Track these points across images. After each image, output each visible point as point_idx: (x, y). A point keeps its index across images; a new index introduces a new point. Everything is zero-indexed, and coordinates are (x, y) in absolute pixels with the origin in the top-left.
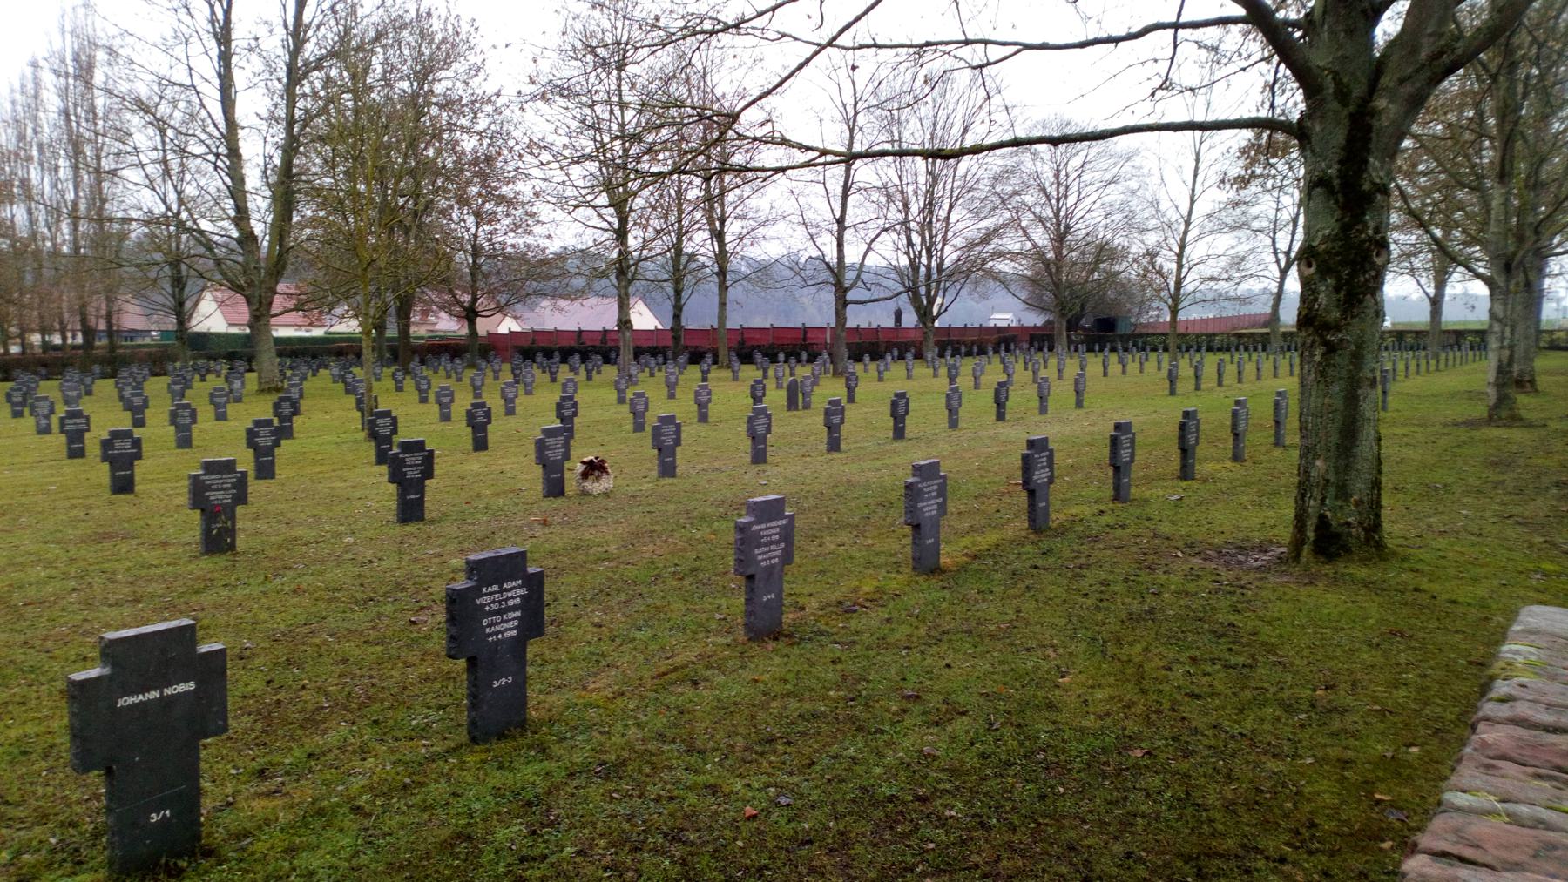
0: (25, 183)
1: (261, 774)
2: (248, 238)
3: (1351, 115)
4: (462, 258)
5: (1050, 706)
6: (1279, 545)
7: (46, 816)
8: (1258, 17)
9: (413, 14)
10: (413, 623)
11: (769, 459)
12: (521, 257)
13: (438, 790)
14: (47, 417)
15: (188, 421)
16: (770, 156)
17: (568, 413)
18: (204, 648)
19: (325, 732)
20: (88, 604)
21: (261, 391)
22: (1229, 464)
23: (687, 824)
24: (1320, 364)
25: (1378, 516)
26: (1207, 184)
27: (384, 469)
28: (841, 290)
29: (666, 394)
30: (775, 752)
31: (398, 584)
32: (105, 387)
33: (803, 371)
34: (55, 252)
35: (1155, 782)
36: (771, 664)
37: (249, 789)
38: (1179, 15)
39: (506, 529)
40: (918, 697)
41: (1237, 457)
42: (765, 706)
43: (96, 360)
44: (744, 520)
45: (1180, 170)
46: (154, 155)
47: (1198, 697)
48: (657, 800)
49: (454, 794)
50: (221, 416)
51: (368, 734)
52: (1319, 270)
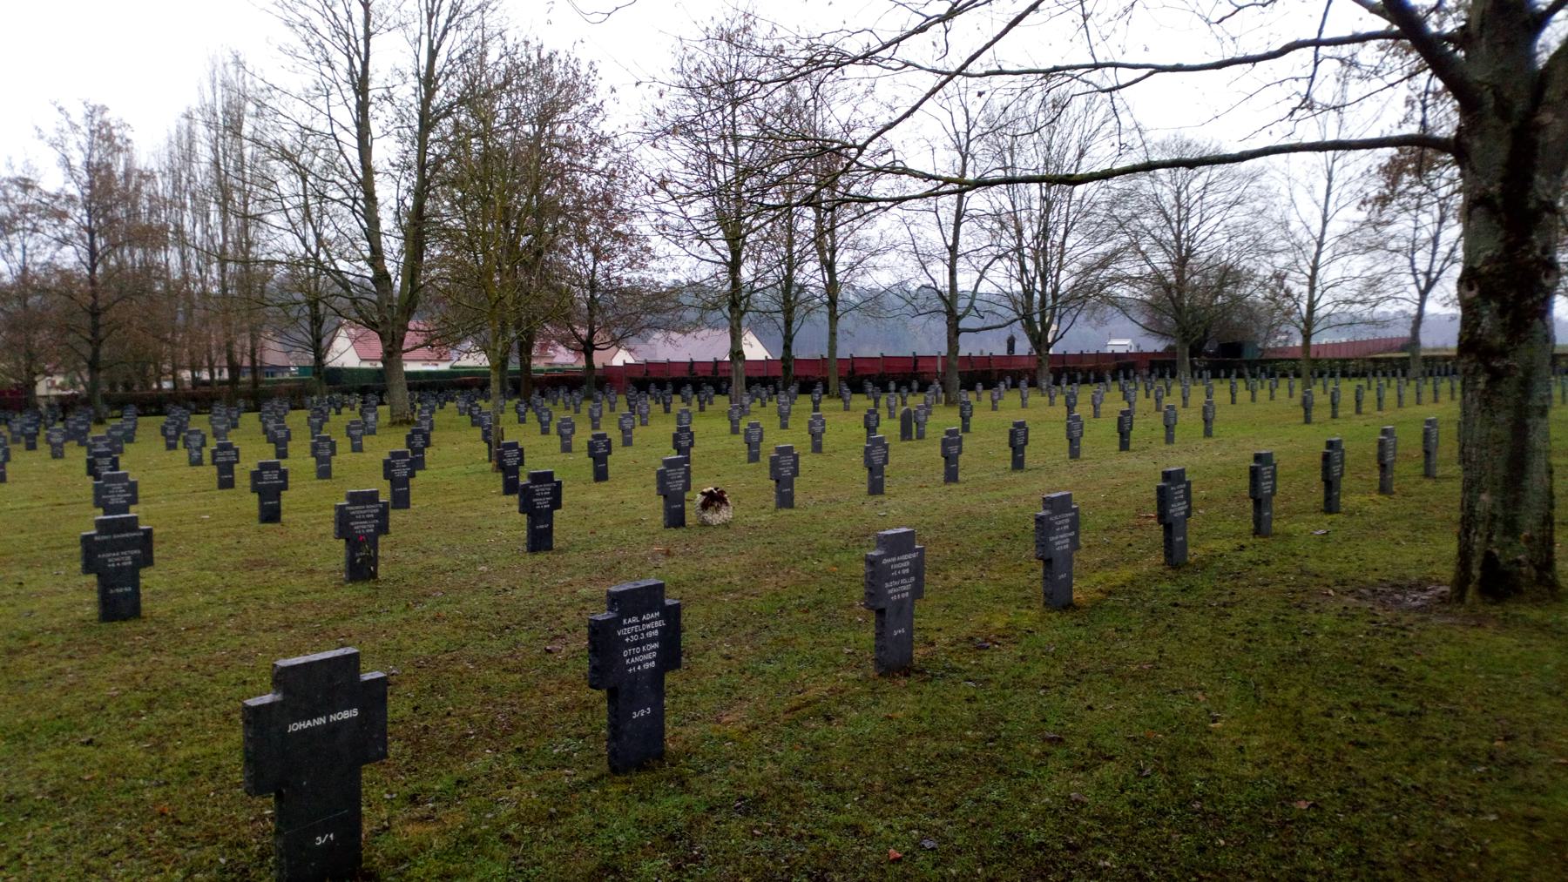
0: (179, 230)
1: (413, 799)
2: (382, 278)
3: (1514, 131)
4: (581, 295)
5: (1203, 753)
6: (1439, 583)
7: (216, 836)
8: (1408, 28)
9: (535, 60)
10: (549, 651)
11: (886, 490)
12: (634, 291)
13: (584, 820)
14: (199, 449)
15: (328, 452)
16: (884, 186)
17: (684, 443)
18: (366, 677)
19: (471, 759)
20: (244, 629)
21: (393, 424)
22: (1376, 497)
23: (830, 865)
24: (1484, 392)
25: (1551, 553)
26: (1341, 204)
27: (514, 499)
28: (953, 319)
29: (782, 425)
30: (915, 793)
31: (532, 613)
32: (250, 420)
33: (915, 401)
34: (205, 294)
35: (1323, 836)
36: (904, 701)
37: (403, 813)
38: (1320, 32)
39: (631, 560)
40: (1060, 740)
41: (1384, 489)
42: (901, 745)
43: (239, 395)
44: (875, 553)
45: (1310, 190)
46: (296, 201)
47: (1364, 746)
48: (799, 838)
49: (599, 826)
50: (357, 448)
51: (512, 762)
52: (1481, 294)
